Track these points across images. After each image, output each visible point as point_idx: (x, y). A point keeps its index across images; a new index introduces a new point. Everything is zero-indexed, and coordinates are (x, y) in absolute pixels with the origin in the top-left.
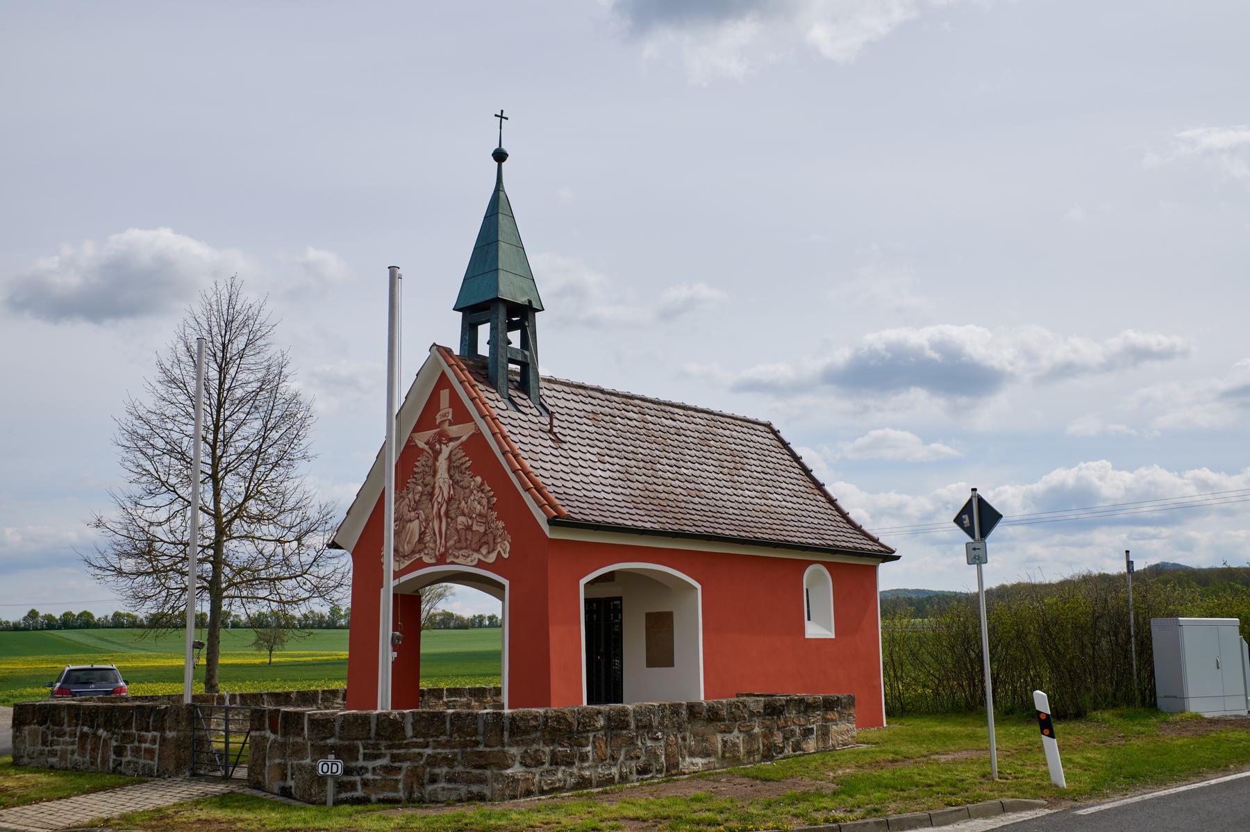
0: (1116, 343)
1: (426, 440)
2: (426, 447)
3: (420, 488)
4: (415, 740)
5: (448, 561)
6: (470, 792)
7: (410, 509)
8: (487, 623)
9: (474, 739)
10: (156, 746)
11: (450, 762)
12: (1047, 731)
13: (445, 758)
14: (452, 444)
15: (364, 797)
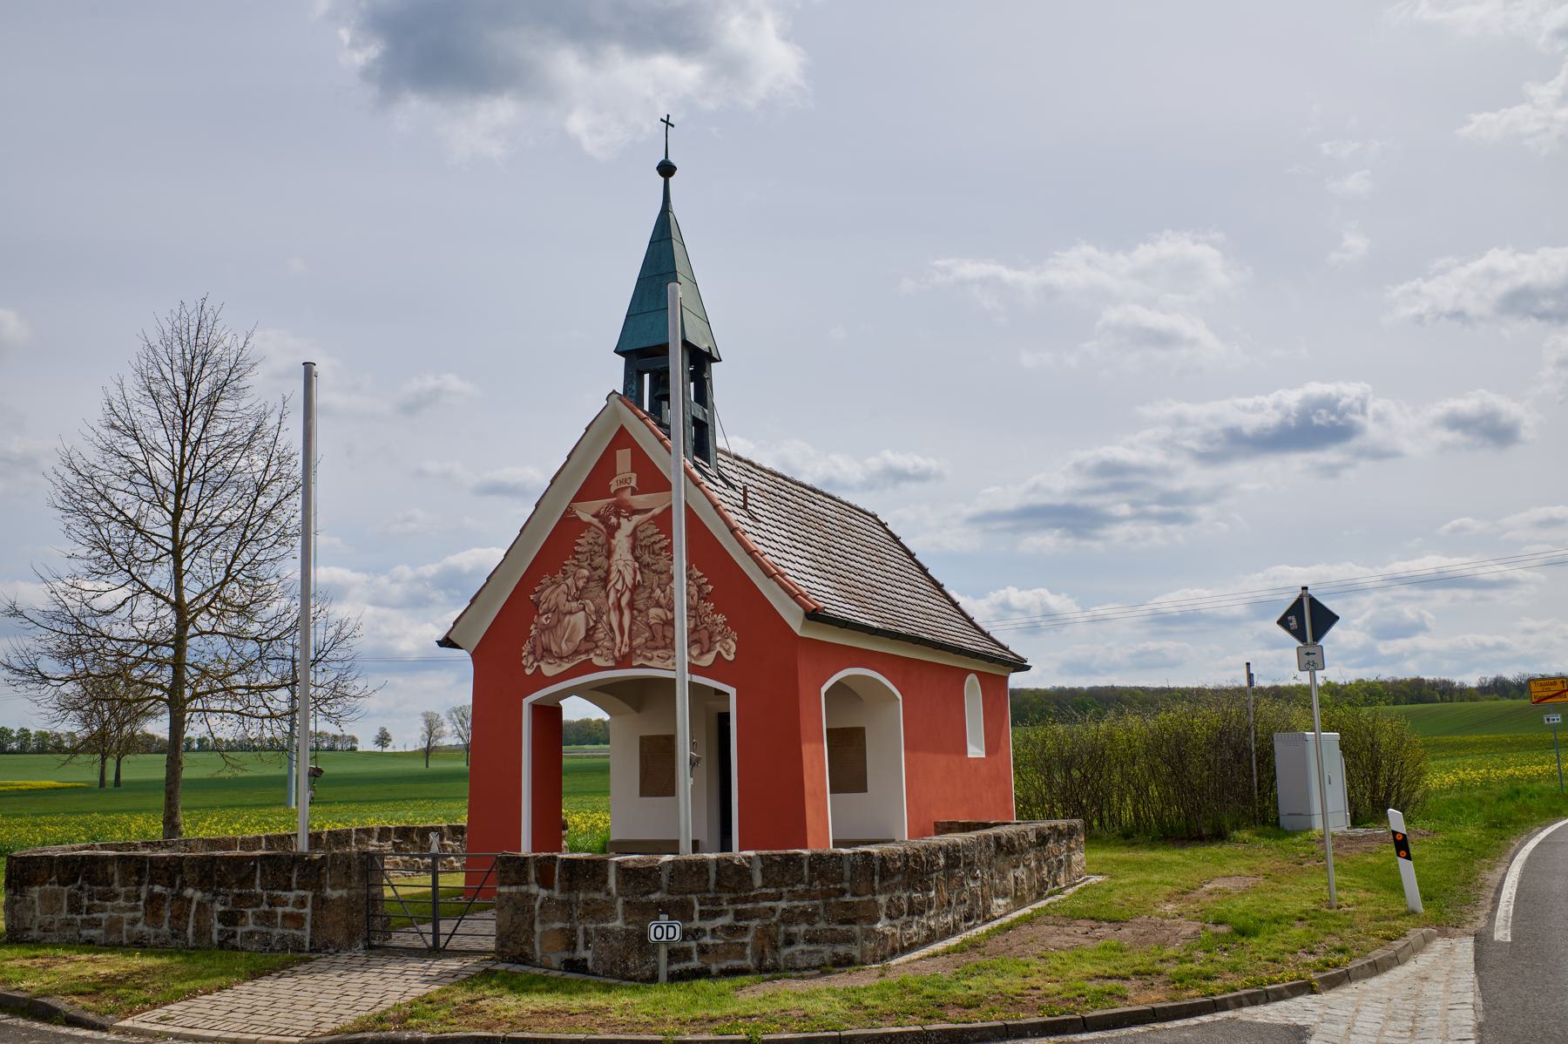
0: (874, 463)
1: (594, 512)
2: (595, 521)
3: (585, 572)
4: (764, 890)
5: (634, 664)
6: (836, 955)
7: (570, 598)
8: (196, 746)
9: (838, 886)
10: (308, 910)
11: (809, 917)
12: (1403, 853)
13: (804, 912)
14: (636, 518)
15: (702, 968)
